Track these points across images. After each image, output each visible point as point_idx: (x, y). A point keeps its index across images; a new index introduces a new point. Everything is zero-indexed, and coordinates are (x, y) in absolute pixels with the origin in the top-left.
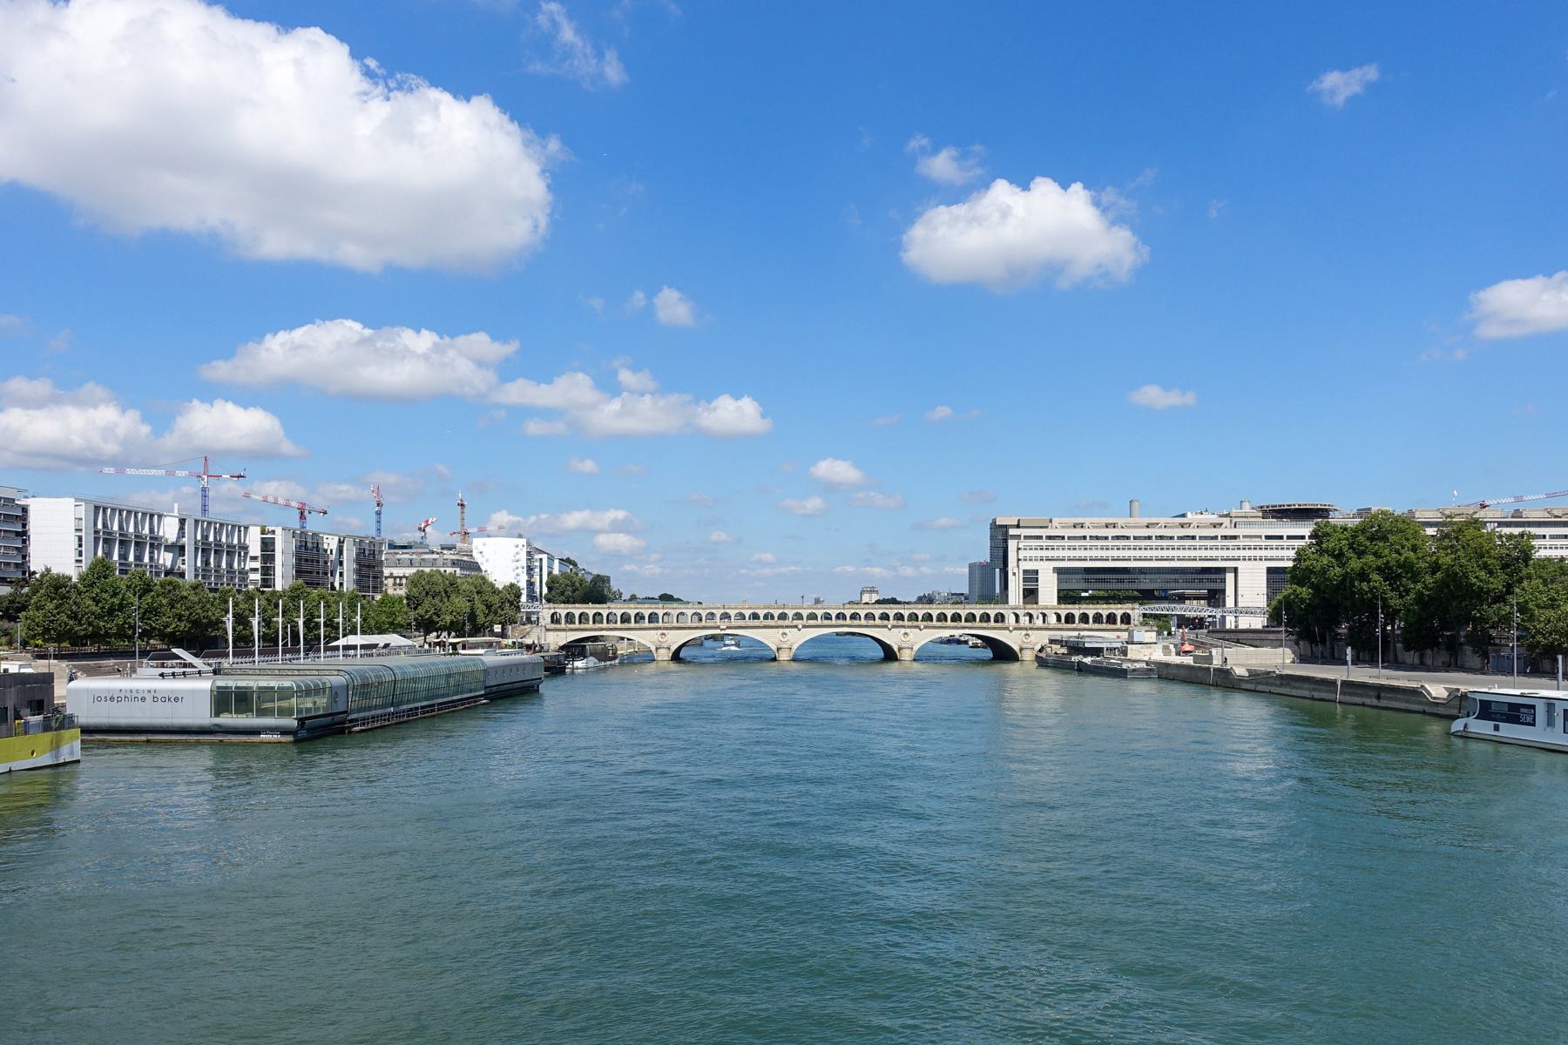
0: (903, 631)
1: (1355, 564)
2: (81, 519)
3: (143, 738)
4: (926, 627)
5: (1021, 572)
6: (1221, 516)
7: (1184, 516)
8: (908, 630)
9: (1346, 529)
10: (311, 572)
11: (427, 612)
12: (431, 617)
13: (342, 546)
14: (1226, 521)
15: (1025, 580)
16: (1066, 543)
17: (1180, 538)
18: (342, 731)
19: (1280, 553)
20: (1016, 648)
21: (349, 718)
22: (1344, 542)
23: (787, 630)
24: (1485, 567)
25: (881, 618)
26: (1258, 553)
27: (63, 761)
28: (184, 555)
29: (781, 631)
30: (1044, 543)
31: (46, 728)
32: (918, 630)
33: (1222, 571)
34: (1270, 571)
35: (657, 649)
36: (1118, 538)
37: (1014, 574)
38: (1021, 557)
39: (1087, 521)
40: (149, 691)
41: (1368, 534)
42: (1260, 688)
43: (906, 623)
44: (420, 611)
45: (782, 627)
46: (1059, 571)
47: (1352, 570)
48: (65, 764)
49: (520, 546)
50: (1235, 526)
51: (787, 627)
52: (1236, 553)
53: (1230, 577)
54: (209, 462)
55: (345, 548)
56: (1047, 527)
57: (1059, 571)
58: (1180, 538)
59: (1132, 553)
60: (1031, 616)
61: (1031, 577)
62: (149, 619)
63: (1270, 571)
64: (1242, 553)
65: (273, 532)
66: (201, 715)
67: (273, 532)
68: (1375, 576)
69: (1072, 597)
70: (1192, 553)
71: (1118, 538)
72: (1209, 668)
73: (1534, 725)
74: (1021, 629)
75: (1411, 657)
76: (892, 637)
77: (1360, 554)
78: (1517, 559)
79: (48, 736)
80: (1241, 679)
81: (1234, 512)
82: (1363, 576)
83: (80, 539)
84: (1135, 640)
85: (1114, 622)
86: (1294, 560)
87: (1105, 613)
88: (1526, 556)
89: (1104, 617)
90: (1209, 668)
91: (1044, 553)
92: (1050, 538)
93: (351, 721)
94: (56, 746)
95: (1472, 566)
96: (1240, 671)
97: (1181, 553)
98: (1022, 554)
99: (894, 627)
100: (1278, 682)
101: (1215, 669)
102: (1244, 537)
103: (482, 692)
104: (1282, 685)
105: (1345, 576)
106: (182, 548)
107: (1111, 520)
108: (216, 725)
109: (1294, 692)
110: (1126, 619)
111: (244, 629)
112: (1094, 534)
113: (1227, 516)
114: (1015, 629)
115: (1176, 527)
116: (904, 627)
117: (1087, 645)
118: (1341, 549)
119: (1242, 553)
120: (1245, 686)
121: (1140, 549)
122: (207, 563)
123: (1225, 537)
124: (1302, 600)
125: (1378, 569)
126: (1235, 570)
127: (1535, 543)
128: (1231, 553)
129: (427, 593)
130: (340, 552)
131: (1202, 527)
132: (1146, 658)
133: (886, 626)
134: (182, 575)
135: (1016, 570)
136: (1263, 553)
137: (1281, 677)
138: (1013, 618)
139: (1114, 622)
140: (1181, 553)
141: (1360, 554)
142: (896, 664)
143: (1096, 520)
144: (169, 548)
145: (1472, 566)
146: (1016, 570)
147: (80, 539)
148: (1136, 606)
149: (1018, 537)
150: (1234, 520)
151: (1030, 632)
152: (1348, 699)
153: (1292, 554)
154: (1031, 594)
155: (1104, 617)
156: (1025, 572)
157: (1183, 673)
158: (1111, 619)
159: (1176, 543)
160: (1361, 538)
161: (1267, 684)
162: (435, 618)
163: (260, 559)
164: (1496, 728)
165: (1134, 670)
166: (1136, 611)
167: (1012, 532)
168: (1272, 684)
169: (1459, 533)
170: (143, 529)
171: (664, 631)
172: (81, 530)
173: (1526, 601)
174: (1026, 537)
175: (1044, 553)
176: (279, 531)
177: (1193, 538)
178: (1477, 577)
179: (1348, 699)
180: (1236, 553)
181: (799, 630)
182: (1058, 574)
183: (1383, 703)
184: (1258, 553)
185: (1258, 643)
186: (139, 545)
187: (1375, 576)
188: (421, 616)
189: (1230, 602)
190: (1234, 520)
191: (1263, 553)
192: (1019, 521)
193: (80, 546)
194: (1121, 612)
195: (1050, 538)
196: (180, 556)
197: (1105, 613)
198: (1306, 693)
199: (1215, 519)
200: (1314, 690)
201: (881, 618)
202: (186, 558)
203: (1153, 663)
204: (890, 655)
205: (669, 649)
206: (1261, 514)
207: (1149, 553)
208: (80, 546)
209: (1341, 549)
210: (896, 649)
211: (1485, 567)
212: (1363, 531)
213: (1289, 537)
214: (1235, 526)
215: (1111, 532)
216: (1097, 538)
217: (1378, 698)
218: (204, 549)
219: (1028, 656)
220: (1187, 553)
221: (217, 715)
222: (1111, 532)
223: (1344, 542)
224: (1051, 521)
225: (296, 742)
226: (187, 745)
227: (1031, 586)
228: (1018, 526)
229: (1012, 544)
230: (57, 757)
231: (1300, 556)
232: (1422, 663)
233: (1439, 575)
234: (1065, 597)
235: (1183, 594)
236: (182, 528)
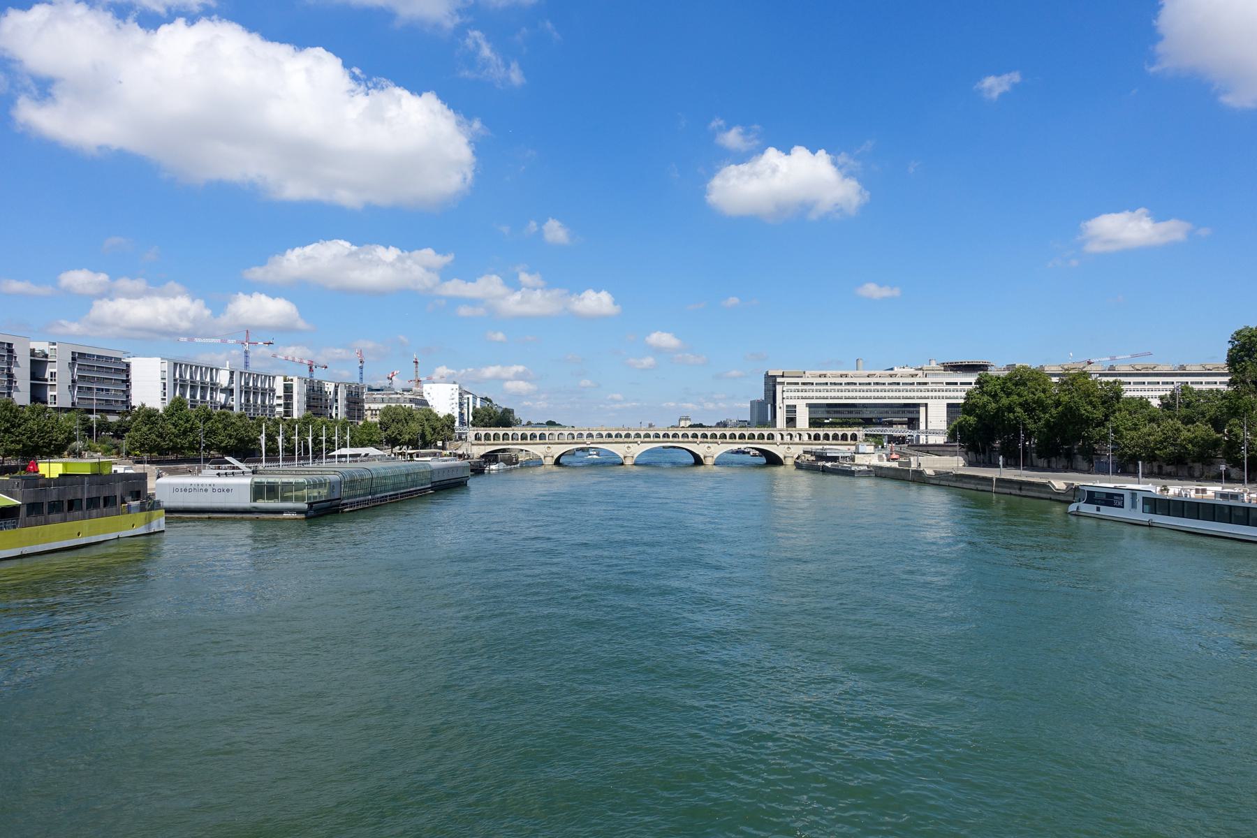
0: (707, 445)
1: (1005, 401)
2: (165, 371)
3: (206, 516)
4: (722, 443)
5: (785, 406)
6: (916, 370)
7: (892, 369)
8: (710, 445)
9: (999, 378)
10: (317, 407)
11: (393, 432)
12: (395, 436)
13: (337, 390)
14: (920, 373)
15: (787, 412)
16: (814, 387)
17: (890, 384)
18: (337, 512)
19: (955, 394)
20: (782, 457)
21: (342, 502)
22: (997, 387)
23: (630, 445)
24: (1091, 403)
25: (692, 437)
26: (941, 394)
27: (153, 531)
28: (233, 395)
29: (627, 445)
30: (800, 387)
31: (142, 509)
32: (716, 445)
33: (918, 405)
34: (949, 405)
35: (545, 457)
36: (848, 384)
37: (780, 408)
38: (785, 396)
39: (828, 373)
40: (210, 485)
41: (1014, 382)
42: (942, 483)
43: (709, 440)
44: (389, 432)
45: (627, 443)
46: (810, 406)
47: (1003, 405)
48: (155, 533)
49: (455, 389)
50: (926, 376)
51: (630, 443)
52: (927, 394)
53: (922, 410)
54: (249, 334)
55: (339, 390)
56: (802, 377)
57: (810, 406)
58: (890, 384)
59: (873, 394)
60: (791, 435)
61: (791, 409)
62: (210, 437)
63: (949, 405)
64: (930, 394)
65: (292, 380)
66: (245, 501)
67: (292, 380)
68: (1018, 409)
69: (817, 423)
70: (898, 394)
71: (848, 384)
72: (909, 470)
73: (1123, 507)
74: (785, 444)
75: (1042, 462)
76: (700, 449)
77: (1008, 395)
78: (1112, 398)
79: (143, 514)
80: (930, 477)
81: (925, 367)
82: (1010, 409)
83: (164, 384)
84: (860, 451)
85: (846, 440)
86: (965, 399)
87: (840, 434)
88: (1118, 396)
89: (840, 436)
90: (909, 470)
91: (800, 394)
92: (803, 384)
93: (343, 505)
94: (148, 521)
95: (1082, 402)
96: (929, 472)
97: (891, 394)
98: (785, 395)
99: (701, 442)
100: (954, 479)
101: (912, 471)
102: (932, 383)
103: (430, 486)
104: (956, 481)
105: (999, 409)
106: (232, 391)
107: (824, 372)
108: (254, 507)
109: (965, 486)
110: (854, 437)
111: (273, 444)
112: (833, 382)
113: (921, 369)
114: (781, 444)
115: (838, 377)
116: (707, 442)
117: (828, 455)
118: (996, 391)
119: (930, 394)
120: (932, 481)
121: (863, 391)
122: (248, 400)
123: (919, 384)
124: (970, 425)
125: (1020, 404)
126: (926, 405)
127: (1124, 387)
128: (923, 394)
129: (393, 420)
130: (336, 393)
131: (883, 377)
132: (867, 463)
133: (696, 442)
134: (232, 408)
135: (781, 405)
136: (944, 394)
137: (956, 475)
138: (779, 437)
139: (846, 440)
140: (891, 394)
141: (1008, 395)
142: (702, 467)
143: (834, 372)
144: (223, 391)
145: (1082, 402)
146: (781, 405)
147: (164, 384)
148: (861, 429)
149: (783, 383)
150: (925, 372)
151: (790, 446)
152: (1000, 490)
153: (963, 394)
154: (791, 421)
155: (840, 436)
156: (787, 406)
157: (892, 473)
158: (844, 437)
159: (887, 387)
160: (1009, 384)
161: (947, 480)
162: (399, 437)
163: (283, 398)
164: (1098, 509)
165: (859, 471)
166: (861, 432)
167: (779, 380)
168: (950, 481)
169: (1075, 381)
170: (206, 378)
171: (550, 446)
172: (165, 379)
173: (1118, 426)
174: (788, 384)
175: (800, 394)
176: (295, 379)
177: (898, 384)
178: (1085, 410)
179: (1000, 490)
180: (927, 394)
181: (639, 445)
182: (809, 407)
183: (1024, 493)
184: (941, 394)
185: (941, 453)
186: (203, 389)
187: (1018, 409)
188: (390, 436)
189: (922, 426)
190: (925, 372)
191: (944, 394)
192: (783, 373)
193: (165, 389)
194: (512, 432)
195: (803, 384)
196: (230, 396)
197: (840, 434)
198: (972, 486)
199: (912, 371)
200: (978, 484)
201: (692, 437)
202: (234, 397)
203: (871, 466)
204: (698, 461)
205: (553, 457)
206: (943, 368)
207: (869, 394)
208: (165, 389)
209: (996, 391)
210: (702, 457)
211: (1091, 403)
212: (1010, 379)
213: (961, 384)
214: (926, 376)
215: (844, 380)
216: (835, 384)
217: (1020, 489)
218: (246, 391)
219: (789, 462)
220: (865, 394)
221: (255, 500)
222: (844, 380)
223: (997, 387)
224: (804, 373)
225: (307, 518)
226: (235, 520)
227: (791, 416)
228: (783, 376)
229: (779, 388)
230: (149, 529)
231: (969, 396)
232: (1049, 466)
233: (1060, 408)
234: (814, 423)
235: (892, 420)
236: (231, 377)
